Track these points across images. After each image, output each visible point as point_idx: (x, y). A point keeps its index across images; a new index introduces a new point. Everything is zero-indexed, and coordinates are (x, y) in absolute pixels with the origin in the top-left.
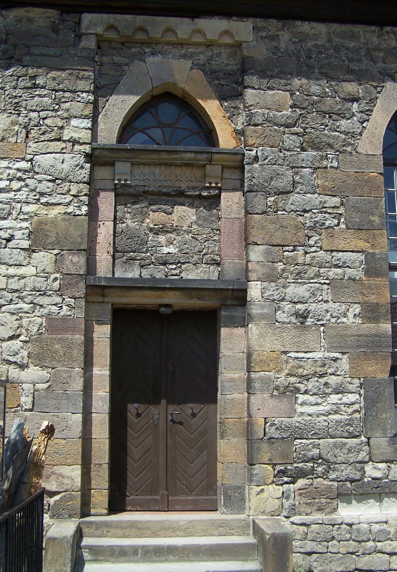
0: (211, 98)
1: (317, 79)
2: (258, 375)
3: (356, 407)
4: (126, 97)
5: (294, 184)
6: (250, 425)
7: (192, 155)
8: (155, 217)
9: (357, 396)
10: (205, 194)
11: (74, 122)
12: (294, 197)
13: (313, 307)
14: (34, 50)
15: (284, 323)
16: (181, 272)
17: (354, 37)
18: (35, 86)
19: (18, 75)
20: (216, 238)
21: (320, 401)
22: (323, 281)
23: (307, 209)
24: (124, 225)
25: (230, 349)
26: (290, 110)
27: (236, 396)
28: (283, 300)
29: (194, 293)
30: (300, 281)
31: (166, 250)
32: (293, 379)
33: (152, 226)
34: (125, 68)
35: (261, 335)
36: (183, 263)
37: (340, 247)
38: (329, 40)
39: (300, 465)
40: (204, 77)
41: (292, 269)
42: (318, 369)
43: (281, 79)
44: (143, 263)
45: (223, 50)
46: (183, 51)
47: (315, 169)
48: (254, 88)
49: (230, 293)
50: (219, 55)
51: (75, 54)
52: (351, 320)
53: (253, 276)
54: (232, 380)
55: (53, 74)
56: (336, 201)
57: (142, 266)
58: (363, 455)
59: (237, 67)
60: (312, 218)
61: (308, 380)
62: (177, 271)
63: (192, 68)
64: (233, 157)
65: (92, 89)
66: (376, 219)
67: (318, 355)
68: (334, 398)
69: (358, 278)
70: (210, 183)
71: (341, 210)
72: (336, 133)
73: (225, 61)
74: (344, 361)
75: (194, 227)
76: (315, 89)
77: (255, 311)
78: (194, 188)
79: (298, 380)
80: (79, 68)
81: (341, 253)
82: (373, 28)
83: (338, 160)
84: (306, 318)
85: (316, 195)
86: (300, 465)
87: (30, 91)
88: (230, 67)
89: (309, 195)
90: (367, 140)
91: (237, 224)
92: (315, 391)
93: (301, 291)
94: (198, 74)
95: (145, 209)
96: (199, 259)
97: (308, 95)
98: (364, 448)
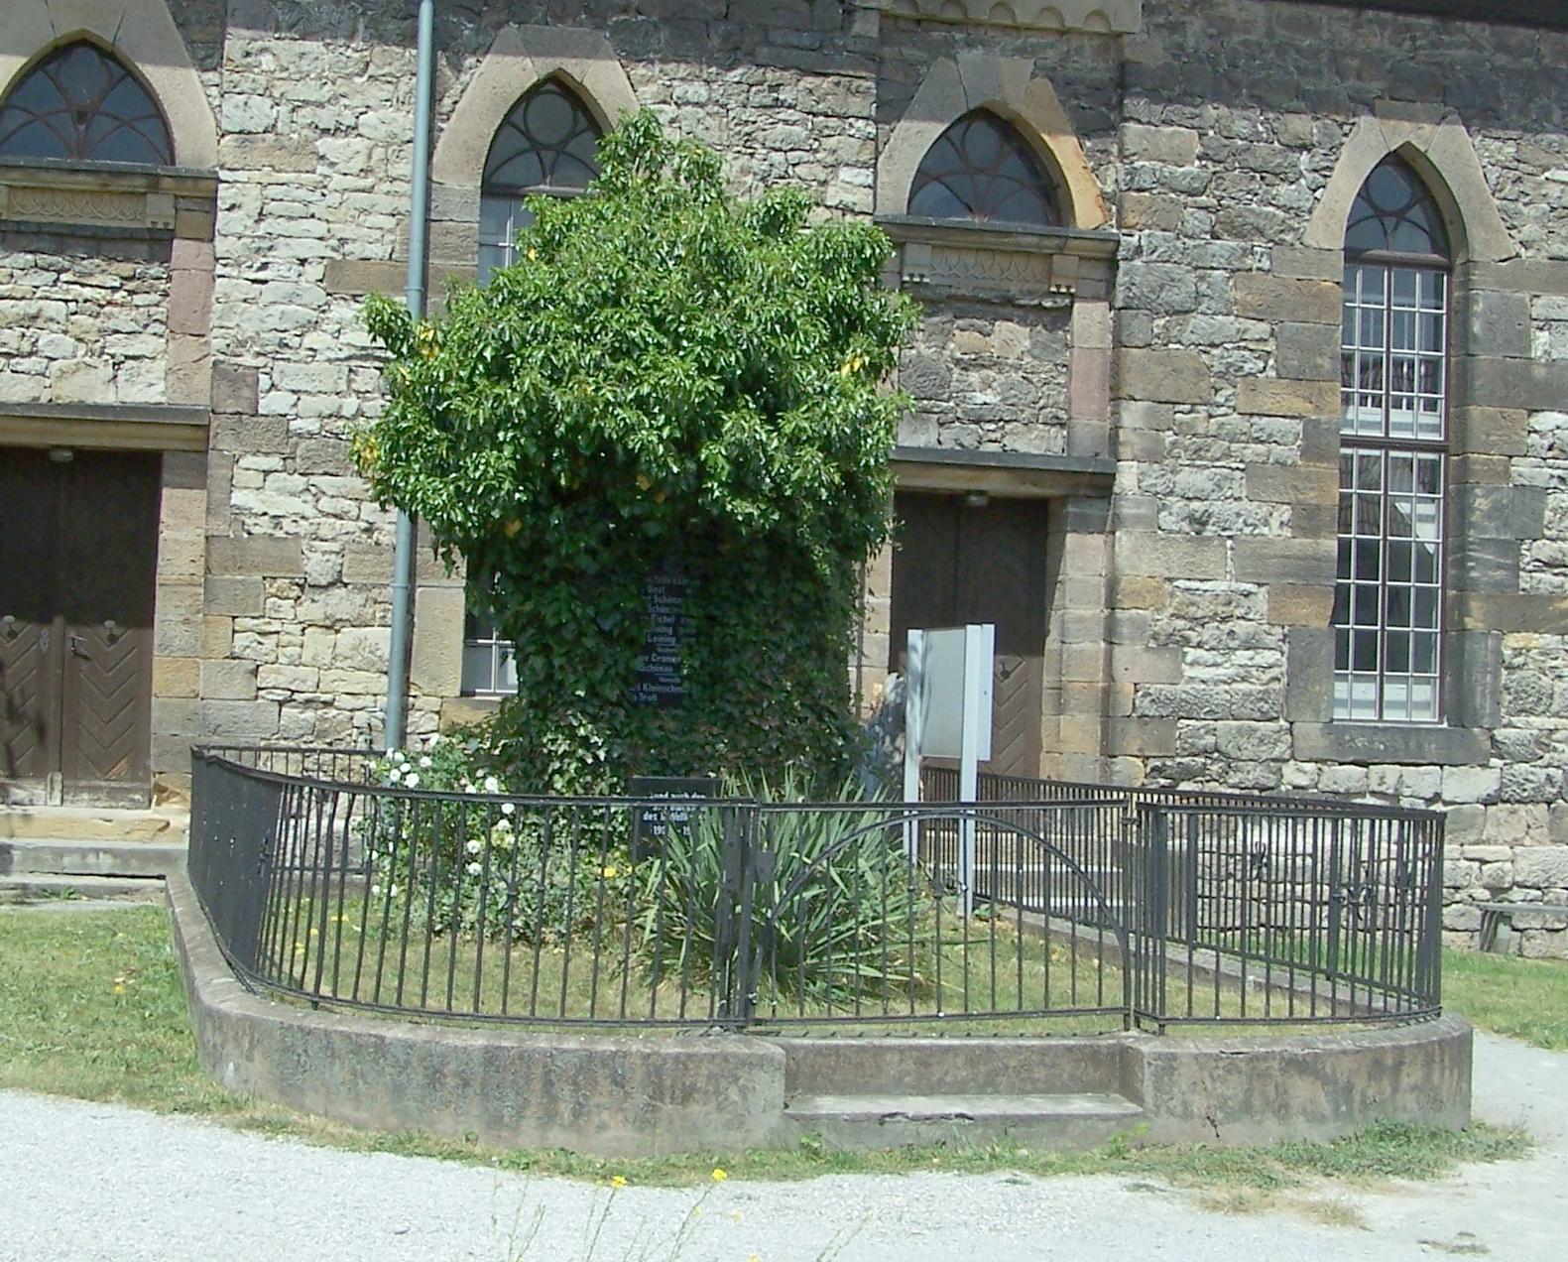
0: (1065, 133)
1: (1246, 108)
2: (1128, 613)
3: (1275, 672)
4: (923, 125)
5: (1198, 296)
6: (1108, 695)
7: (1034, 240)
8: (964, 340)
9: (1278, 655)
10: (1048, 304)
11: (845, 174)
12: (1196, 321)
13: (1216, 507)
14: (777, 37)
15: (1170, 532)
16: (1003, 436)
17: (1311, 28)
18: (778, 104)
19: (751, 81)
20: (1061, 380)
21: (1220, 660)
22: (1234, 465)
23: (1217, 342)
24: (914, 352)
25: (1080, 569)
26: (1197, 163)
27: (1087, 645)
28: (1171, 493)
29: (1030, 476)
30: (1198, 463)
31: (980, 398)
32: (1180, 623)
33: (958, 355)
34: (923, 70)
35: (1135, 551)
36: (1007, 422)
37: (1265, 410)
38: (1270, 34)
39: (1184, 760)
40: (1054, 94)
41: (1187, 442)
42: (1220, 609)
43: (1185, 105)
44: (943, 418)
45: (1086, 41)
46: (1019, 42)
47: (1233, 271)
48: (1139, 122)
49: (1087, 478)
50: (1079, 50)
51: (844, 47)
52: (1276, 531)
53: (1125, 452)
54: (1080, 620)
55: (809, 81)
56: (1263, 328)
57: (941, 425)
58: (1281, 750)
59: (1109, 75)
60: (1222, 357)
61: (1203, 625)
62: (998, 435)
63: (1033, 75)
64: (1100, 245)
65: (873, 113)
66: (1325, 363)
67: (1220, 586)
68: (1242, 656)
69: (1289, 462)
70: (1058, 287)
71: (1271, 346)
72: (1271, 209)
73: (1090, 65)
74: (1260, 596)
75: (1027, 359)
76: (1241, 126)
77: (1127, 510)
78: (1031, 293)
79: (1189, 625)
80: (851, 73)
81: (1266, 419)
82: (1345, 11)
83: (1270, 258)
84: (1204, 524)
85: (1232, 318)
86: (1184, 760)
87: (769, 112)
88: (1096, 75)
89: (1220, 317)
90: (1320, 222)
91: (1099, 359)
92: (1213, 643)
93: (1191, 479)
94: (1043, 86)
95: (948, 326)
96: (1033, 415)
97: (1227, 138)
98: (1284, 738)
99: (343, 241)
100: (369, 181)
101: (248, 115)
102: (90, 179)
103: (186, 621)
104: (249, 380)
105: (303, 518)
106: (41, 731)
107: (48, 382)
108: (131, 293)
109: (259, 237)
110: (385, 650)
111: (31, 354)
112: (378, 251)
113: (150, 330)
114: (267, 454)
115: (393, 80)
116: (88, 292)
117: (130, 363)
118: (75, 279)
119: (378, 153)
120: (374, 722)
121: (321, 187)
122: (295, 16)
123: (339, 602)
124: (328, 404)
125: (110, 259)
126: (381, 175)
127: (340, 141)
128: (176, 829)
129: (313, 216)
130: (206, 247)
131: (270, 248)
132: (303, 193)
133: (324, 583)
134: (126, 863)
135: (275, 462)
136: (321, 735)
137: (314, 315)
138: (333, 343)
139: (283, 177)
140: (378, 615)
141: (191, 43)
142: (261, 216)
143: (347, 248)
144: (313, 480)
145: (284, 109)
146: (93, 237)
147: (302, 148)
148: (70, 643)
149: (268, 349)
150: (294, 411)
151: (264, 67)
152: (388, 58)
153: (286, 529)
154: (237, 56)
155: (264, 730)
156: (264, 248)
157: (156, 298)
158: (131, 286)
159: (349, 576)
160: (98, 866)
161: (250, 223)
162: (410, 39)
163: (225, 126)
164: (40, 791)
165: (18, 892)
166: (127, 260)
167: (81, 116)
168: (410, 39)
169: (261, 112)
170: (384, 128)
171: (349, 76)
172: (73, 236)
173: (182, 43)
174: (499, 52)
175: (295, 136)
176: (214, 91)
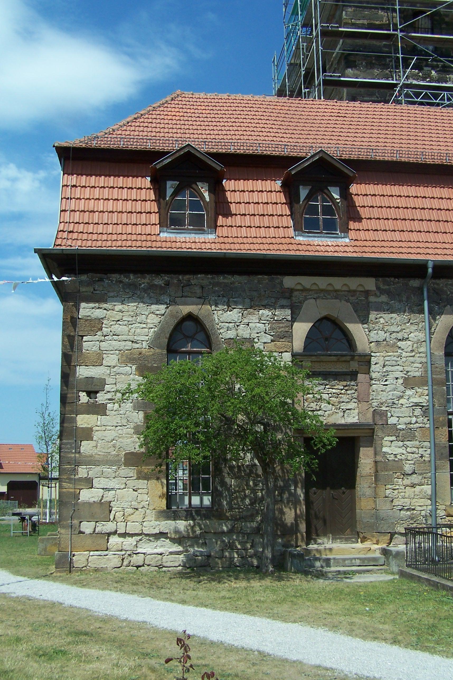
99: (408, 372)
100: (413, 354)
101: (378, 336)
102: (334, 358)
103: (369, 487)
104: (385, 414)
105: (403, 454)
106: (325, 521)
107: (325, 418)
108: (346, 390)
109: (384, 372)
110: (429, 492)
111: (319, 410)
112: (418, 374)
113: (352, 401)
114: (391, 436)
115: (417, 324)
116: (334, 391)
117: (348, 411)
118: (330, 387)
119: (415, 345)
120: (427, 514)
121: (400, 356)
122: (388, 307)
123: (415, 479)
124: (407, 420)
125: (340, 381)
126: (417, 352)
127: (404, 343)
128: (373, 550)
129: (398, 365)
130: (367, 376)
131: (387, 375)
132: (395, 358)
133: (410, 473)
134: (363, 562)
135: (394, 438)
136: (412, 519)
137: (401, 394)
138: (407, 402)
139: (389, 354)
140: (426, 482)
141: (359, 316)
142: (384, 366)
143: (409, 374)
144: (405, 443)
145: (388, 334)
146: (335, 375)
147: (394, 345)
148: (331, 495)
149: (389, 405)
150: (398, 423)
151: (381, 322)
152: (416, 318)
153: (398, 458)
154: (373, 319)
155: (396, 518)
156: (386, 375)
157: (353, 391)
158: (346, 388)
159: (417, 471)
160: (356, 563)
161: (381, 368)
162: (421, 311)
163: (371, 340)
164: (325, 540)
165: (337, 573)
166: (344, 381)
167: (326, 339)
168: (421, 311)
169: (382, 335)
170: (416, 338)
171: (405, 324)
172: (329, 374)
173: (356, 317)
174: (445, 314)
175: (391, 342)
176: (366, 330)
